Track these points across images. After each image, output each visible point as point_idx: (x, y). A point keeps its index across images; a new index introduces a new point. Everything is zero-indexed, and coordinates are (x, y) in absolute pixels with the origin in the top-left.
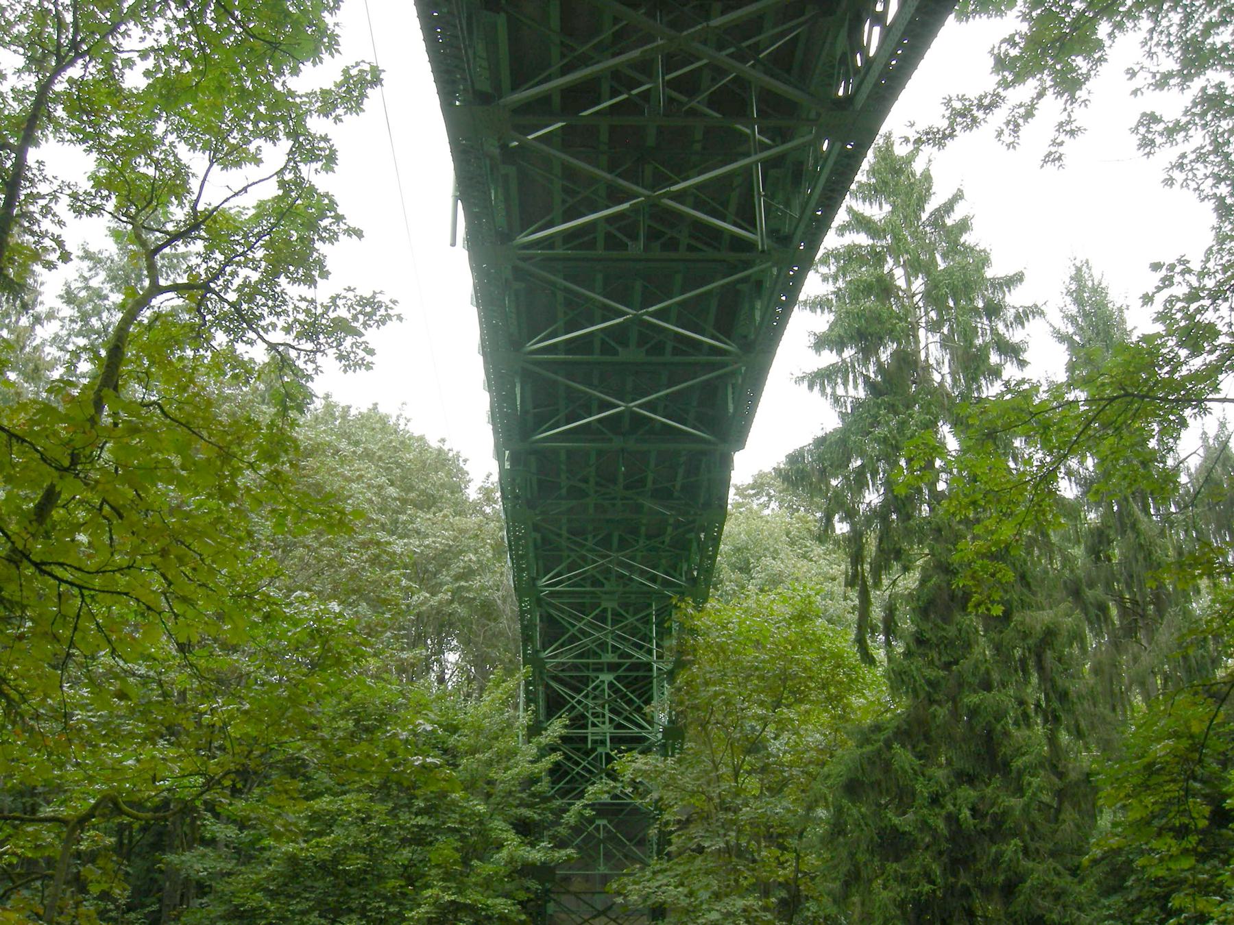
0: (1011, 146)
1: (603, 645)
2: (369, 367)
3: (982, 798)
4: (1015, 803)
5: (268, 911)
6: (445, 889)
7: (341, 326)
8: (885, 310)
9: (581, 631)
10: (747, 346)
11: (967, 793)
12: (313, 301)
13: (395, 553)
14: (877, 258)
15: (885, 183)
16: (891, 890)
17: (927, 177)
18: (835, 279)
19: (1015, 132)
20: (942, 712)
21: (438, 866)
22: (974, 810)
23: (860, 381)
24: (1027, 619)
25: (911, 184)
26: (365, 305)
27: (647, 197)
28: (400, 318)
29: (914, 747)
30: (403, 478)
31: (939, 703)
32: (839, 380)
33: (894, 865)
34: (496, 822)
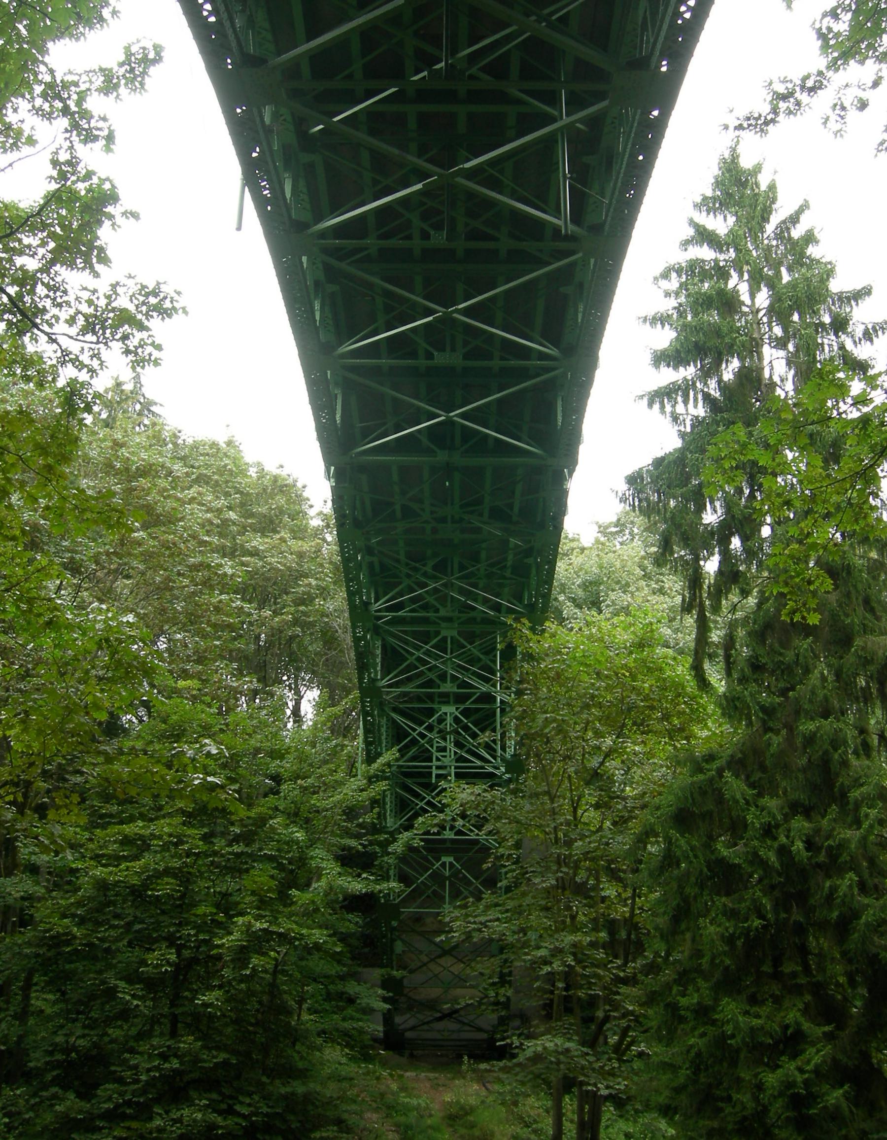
0: (838, 133)
1: (443, 677)
2: (156, 363)
3: (818, 831)
4: (851, 835)
5: (75, 937)
6: (258, 918)
7: (124, 318)
8: (725, 323)
9: (419, 659)
10: (569, 351)
11: (799, 824)
12: (94, 291)
13: (225, 574)
14: (722, 273)
15: (730, 195)
16: (719, 925)
17: (772, 187)
18: (677, 294)
19: (842, 117)
20: (776, 741)
21: (253, 893)
22: (809, 845)
23: (700, 396)
24: (869, 644)
25: (756, 195)
26: (147, 295)
27: (440, 176)
28: (185, 312)
29: (748, 777)
30: (242, 505)
31: (777, 732)
32: (680, 399)
33: (724, 899)
34: (317, 851)
